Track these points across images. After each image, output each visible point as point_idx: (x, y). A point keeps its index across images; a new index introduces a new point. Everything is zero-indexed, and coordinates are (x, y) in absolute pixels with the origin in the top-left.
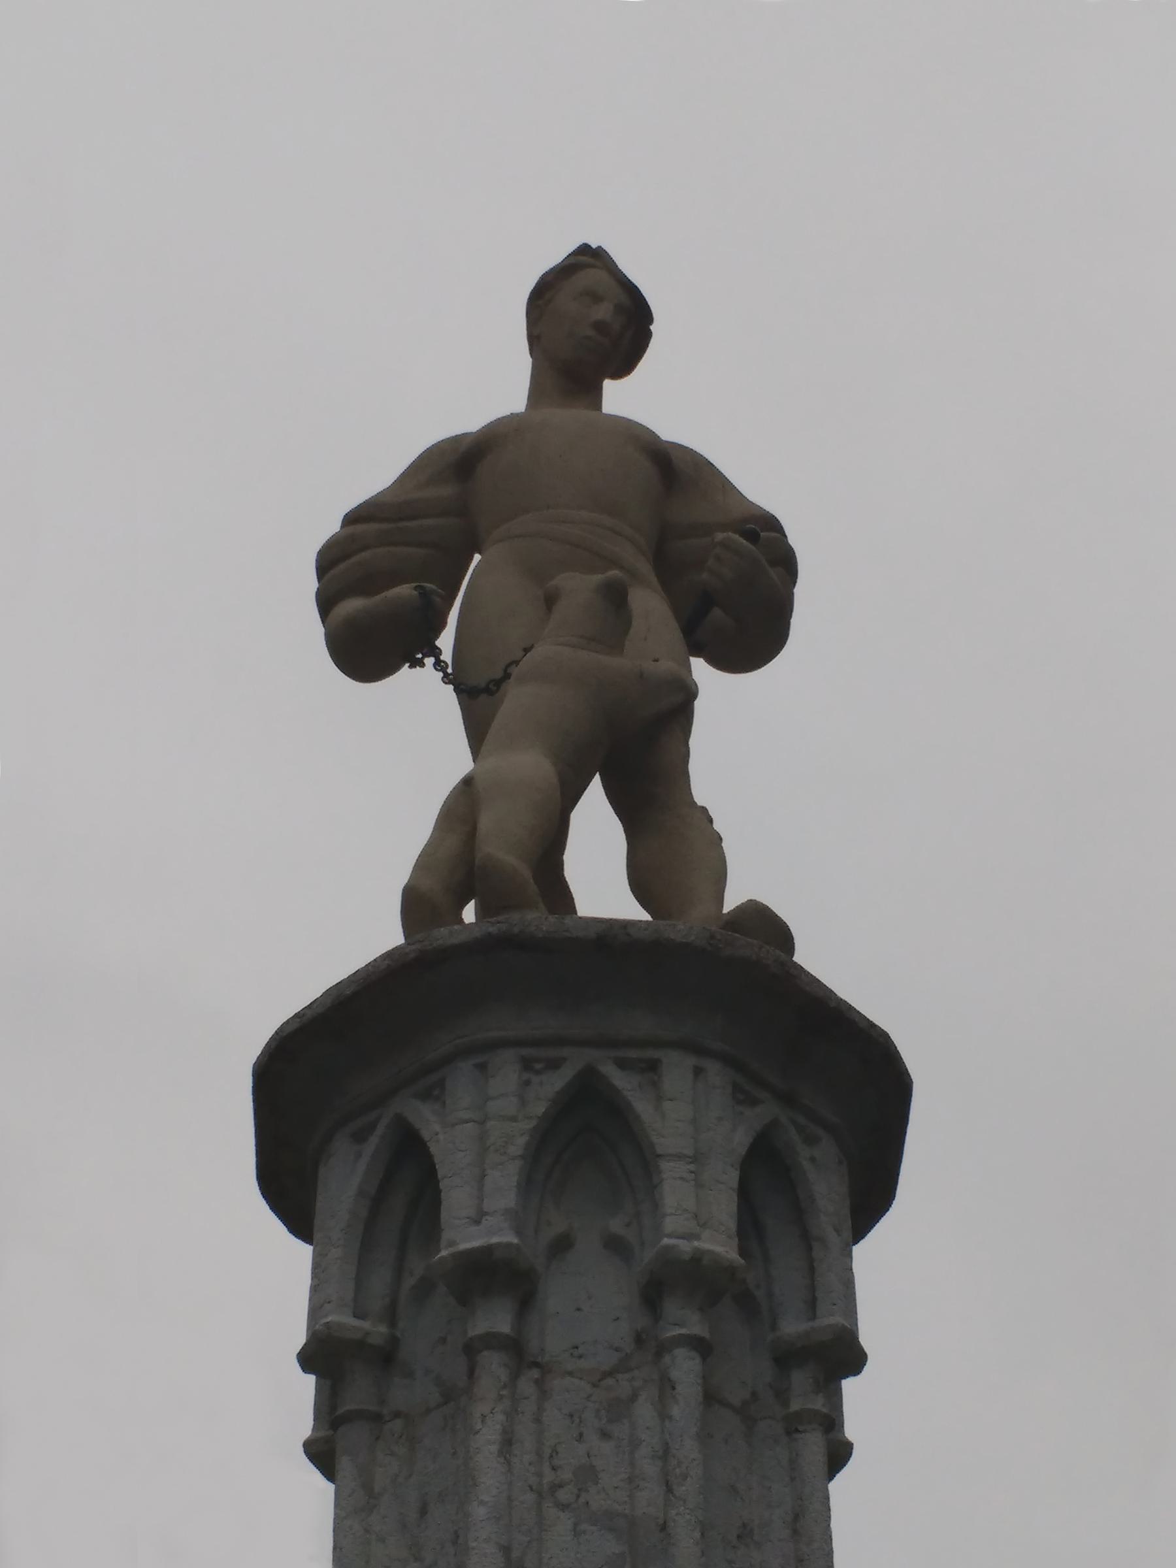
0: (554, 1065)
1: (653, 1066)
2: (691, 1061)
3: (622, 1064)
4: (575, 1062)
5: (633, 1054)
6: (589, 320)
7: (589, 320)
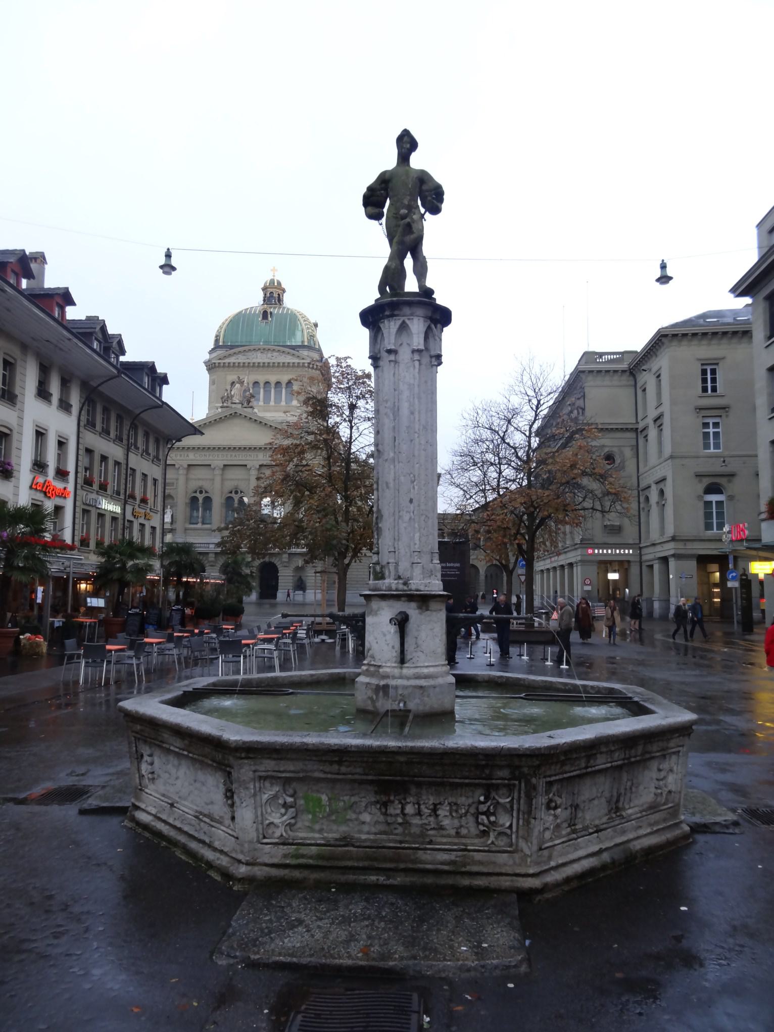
6: (406, 144)
7: (406, 144)
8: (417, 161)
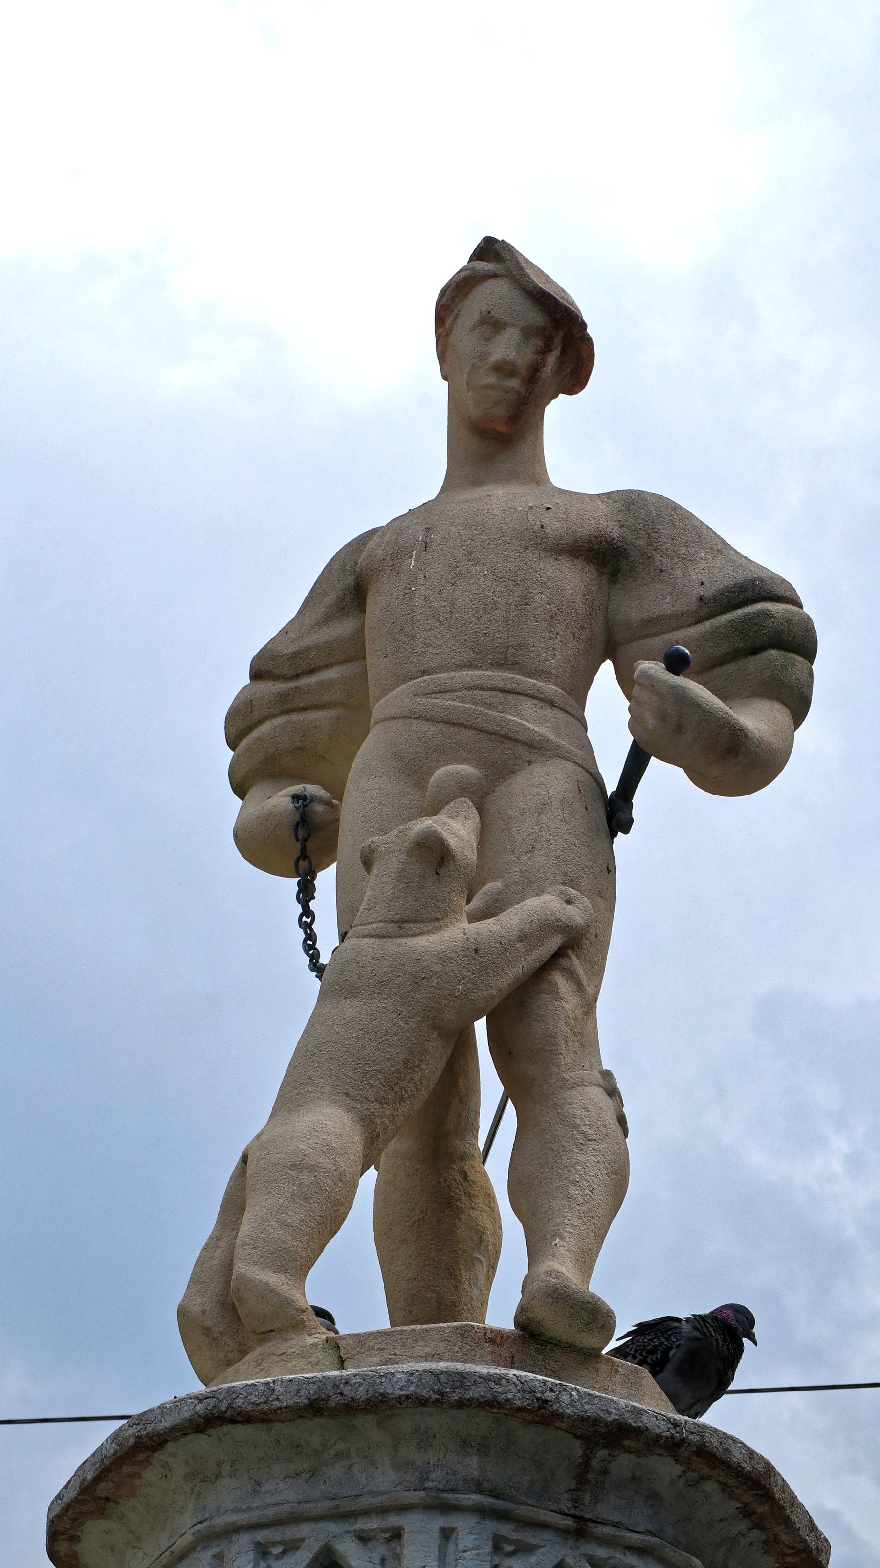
0: (291, 1547)
1: (396, 1535)
2: (439, 1522)
3: (363, 1538)
4: (313, 1537)
5: (371, 1524)
6: (515, 339)
8: (583, 449)
